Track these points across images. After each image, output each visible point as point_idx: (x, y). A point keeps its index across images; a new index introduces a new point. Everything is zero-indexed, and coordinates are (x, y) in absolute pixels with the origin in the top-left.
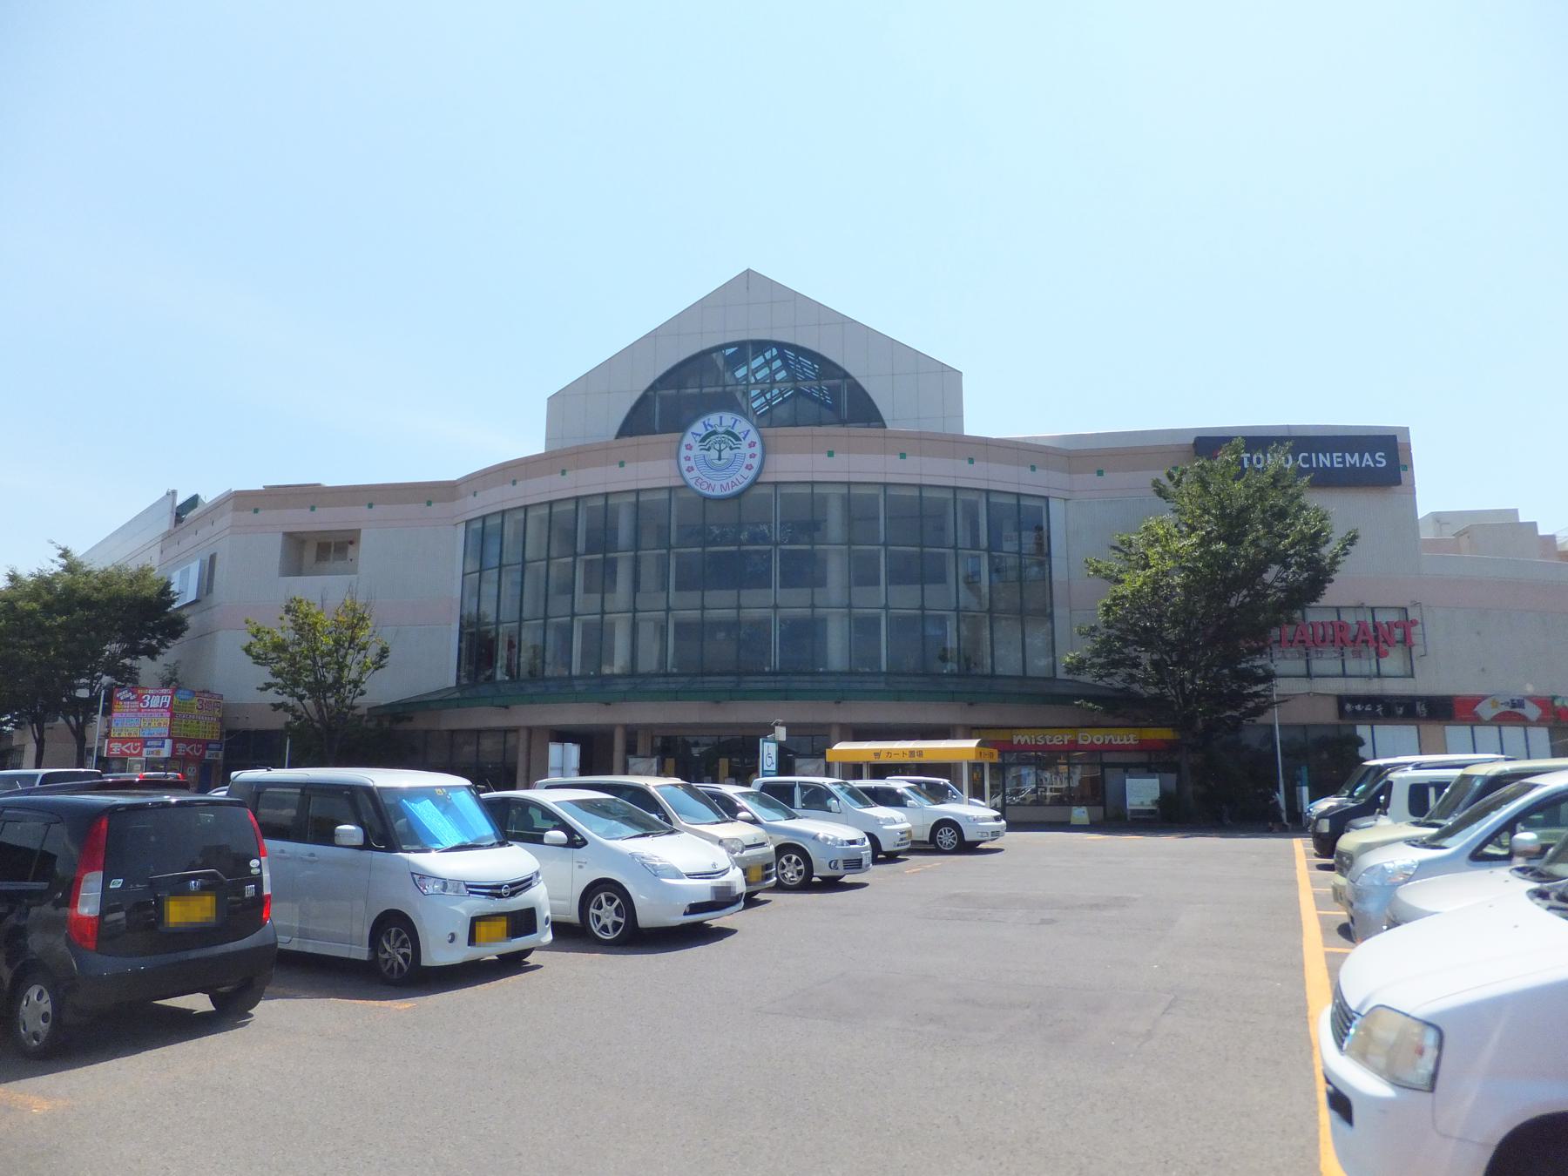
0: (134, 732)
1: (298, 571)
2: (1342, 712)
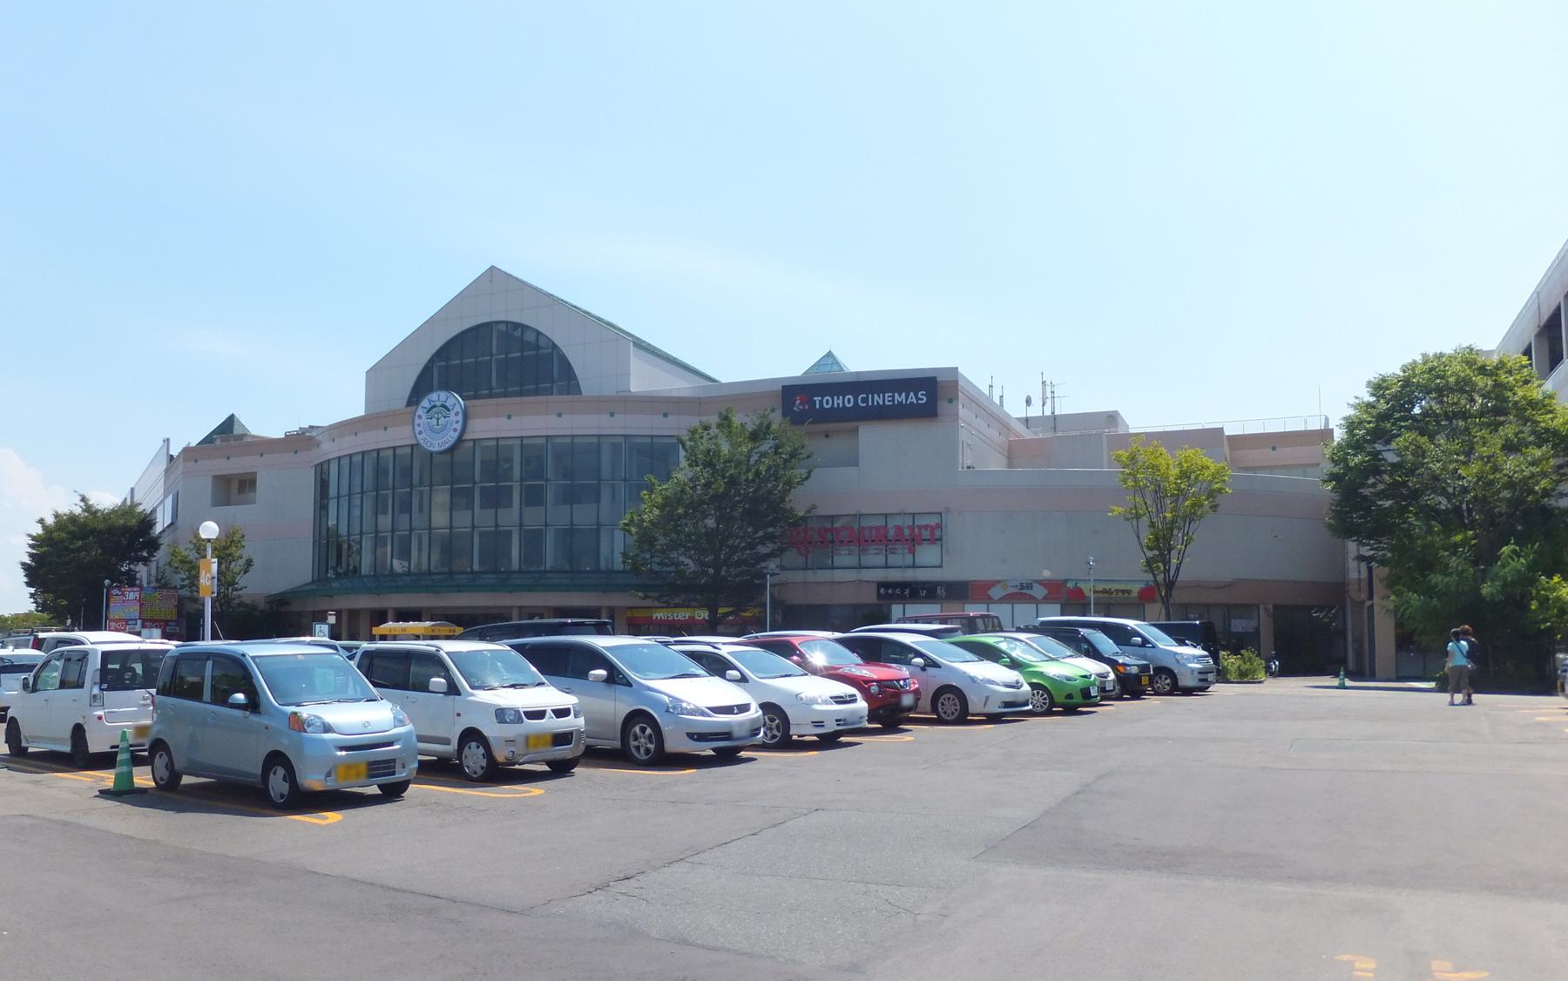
0: (123, 616)
1: (228, 503)
2: (879, 596)
